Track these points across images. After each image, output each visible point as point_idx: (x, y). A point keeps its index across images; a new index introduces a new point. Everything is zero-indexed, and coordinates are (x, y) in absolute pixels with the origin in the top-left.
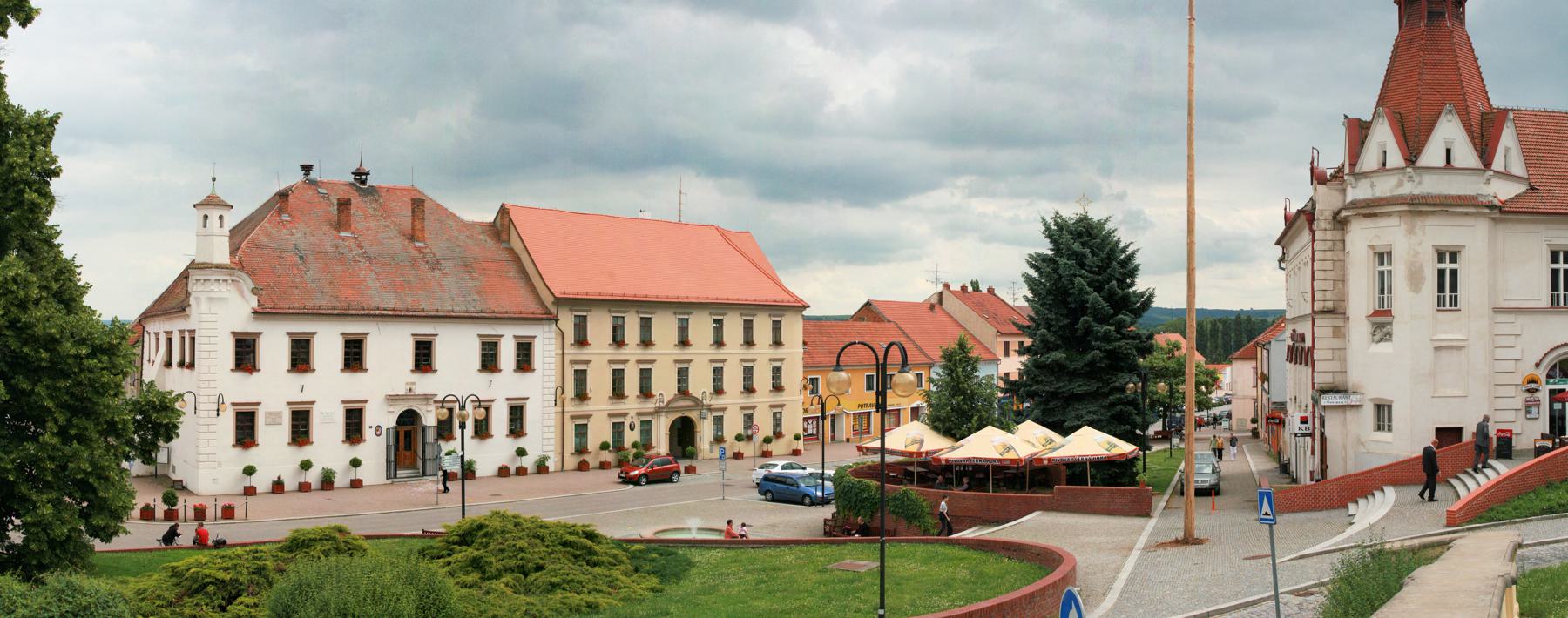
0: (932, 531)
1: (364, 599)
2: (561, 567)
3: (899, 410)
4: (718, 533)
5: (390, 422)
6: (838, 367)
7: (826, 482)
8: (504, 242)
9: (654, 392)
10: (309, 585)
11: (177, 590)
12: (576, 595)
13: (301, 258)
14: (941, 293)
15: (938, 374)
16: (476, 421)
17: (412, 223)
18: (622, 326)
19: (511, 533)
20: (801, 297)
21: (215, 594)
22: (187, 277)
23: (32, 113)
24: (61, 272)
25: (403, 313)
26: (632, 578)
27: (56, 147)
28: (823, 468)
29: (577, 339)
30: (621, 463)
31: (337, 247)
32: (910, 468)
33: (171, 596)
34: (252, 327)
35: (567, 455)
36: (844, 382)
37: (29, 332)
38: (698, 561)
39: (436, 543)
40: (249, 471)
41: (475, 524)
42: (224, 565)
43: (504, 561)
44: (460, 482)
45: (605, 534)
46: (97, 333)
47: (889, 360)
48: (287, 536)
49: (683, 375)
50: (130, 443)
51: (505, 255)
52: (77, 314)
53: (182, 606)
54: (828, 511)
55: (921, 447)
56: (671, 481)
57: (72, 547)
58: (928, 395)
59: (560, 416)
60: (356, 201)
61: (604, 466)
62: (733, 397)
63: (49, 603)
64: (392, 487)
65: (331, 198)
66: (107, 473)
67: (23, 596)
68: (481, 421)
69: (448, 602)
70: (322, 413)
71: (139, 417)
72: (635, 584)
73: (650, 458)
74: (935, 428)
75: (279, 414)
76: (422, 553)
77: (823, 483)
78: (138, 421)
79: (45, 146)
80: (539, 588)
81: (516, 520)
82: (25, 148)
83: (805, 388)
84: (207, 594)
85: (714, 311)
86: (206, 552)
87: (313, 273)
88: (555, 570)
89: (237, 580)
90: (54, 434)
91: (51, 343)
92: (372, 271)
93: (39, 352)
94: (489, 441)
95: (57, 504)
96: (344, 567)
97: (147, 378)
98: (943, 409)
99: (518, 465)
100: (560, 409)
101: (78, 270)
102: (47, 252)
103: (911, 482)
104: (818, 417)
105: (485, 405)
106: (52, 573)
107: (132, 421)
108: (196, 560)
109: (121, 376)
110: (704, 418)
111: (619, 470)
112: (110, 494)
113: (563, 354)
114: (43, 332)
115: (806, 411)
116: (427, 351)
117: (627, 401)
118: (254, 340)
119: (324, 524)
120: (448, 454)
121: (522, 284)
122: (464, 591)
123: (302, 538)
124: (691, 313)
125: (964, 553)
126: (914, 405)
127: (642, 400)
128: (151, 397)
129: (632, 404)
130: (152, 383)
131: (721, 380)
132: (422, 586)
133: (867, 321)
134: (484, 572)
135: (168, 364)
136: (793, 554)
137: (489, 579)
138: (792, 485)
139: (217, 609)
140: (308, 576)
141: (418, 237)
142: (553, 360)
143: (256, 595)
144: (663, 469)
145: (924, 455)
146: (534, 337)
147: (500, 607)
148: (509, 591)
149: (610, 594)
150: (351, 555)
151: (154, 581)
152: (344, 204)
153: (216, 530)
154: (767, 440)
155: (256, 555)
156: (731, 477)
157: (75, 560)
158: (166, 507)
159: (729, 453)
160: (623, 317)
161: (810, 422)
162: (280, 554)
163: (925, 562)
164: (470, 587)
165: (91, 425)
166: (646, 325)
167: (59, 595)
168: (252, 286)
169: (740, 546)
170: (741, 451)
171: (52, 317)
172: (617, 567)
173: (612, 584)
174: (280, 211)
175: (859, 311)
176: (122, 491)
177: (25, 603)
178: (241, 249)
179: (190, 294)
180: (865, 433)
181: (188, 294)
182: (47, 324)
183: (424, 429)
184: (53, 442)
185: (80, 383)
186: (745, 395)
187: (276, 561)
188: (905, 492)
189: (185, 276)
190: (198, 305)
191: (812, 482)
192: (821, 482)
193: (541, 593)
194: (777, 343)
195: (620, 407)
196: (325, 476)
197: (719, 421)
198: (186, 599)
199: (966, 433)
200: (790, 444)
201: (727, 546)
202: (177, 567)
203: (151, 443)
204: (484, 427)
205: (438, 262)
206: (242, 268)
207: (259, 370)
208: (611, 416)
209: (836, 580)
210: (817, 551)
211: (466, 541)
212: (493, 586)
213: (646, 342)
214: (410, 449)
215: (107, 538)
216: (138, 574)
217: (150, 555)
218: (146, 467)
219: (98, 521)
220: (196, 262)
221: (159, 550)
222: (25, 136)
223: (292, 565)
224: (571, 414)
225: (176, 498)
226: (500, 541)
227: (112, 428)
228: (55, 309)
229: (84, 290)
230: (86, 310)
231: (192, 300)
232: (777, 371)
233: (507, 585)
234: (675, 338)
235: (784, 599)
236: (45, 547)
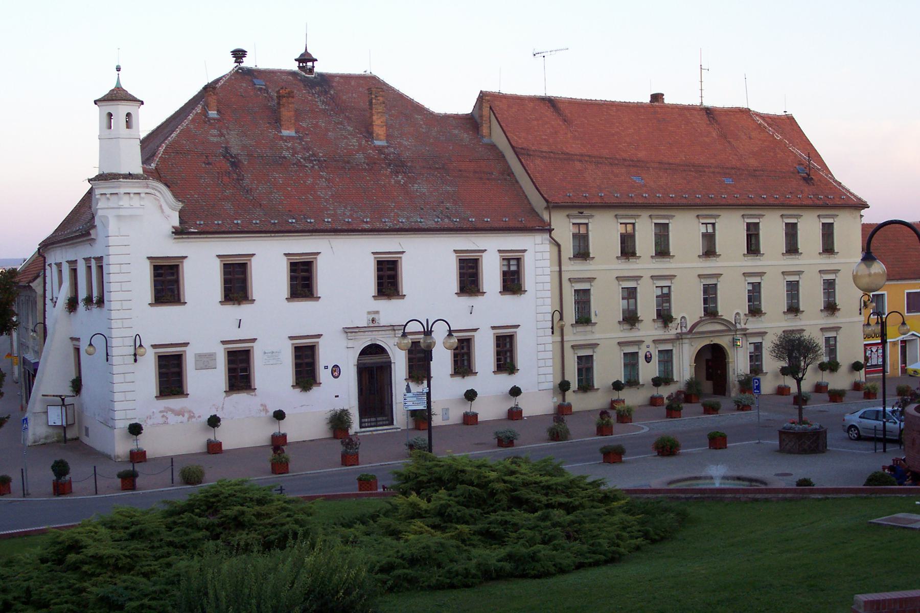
9: (674, 315)
34: (171, 249)
49: (710, 293)
100: (559, 339)
113: (560, 271)
142: (548, 279)
160: (587, 224)
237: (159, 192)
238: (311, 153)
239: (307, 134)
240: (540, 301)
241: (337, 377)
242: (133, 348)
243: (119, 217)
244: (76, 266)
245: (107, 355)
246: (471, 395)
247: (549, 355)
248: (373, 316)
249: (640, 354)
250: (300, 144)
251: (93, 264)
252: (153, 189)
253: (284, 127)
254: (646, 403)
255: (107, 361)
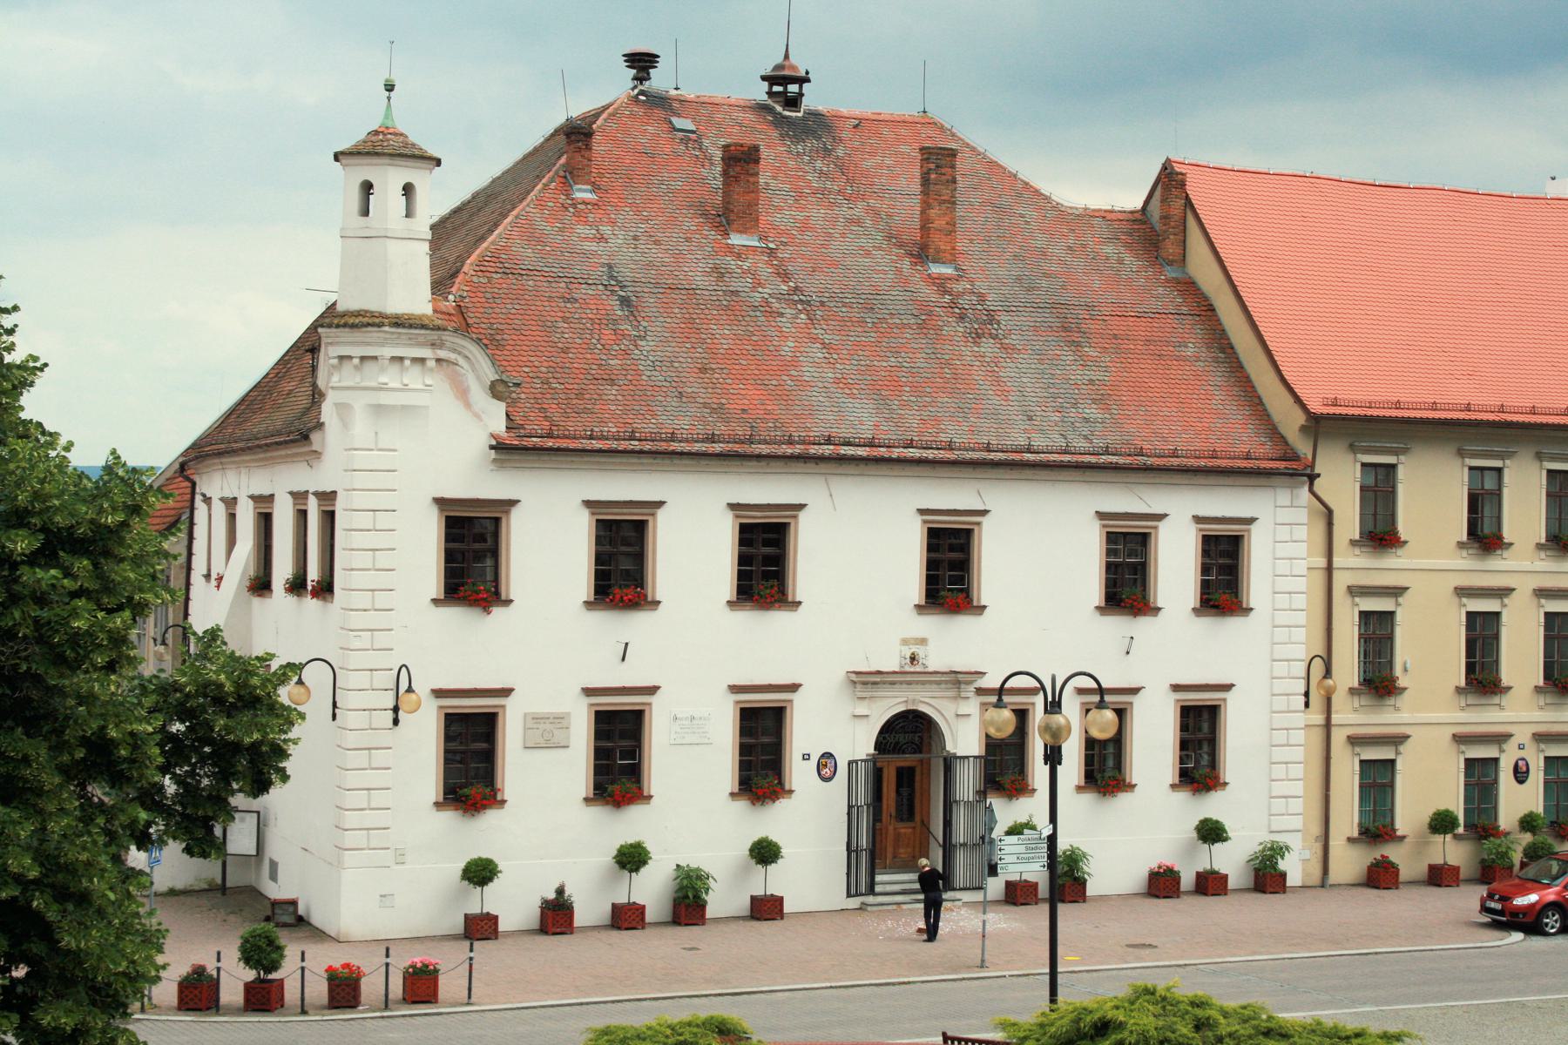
34: (487, 485)
70: (676, 718)
113: (1329, 569)
142: (1301, 584)
160: (1499, 470)
237: (466, 357)
238: (791, 284)
240: (1281, 634)
241: (829, 779)
242: (392, 694)
243: (379, 410)
244: (272, 508)
245: (335, 705)
247: (1298, 754)
248: (914, 649)
249: (1502, 763)
251: (313, 509)
252: (454, 351)
254: (1422, 879)
255: (334, 717)
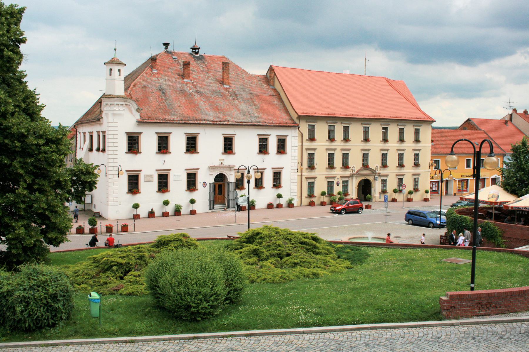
0: (502, 246)
1: (196, 270)
2: (300, 255)
3: (484, 179)
4: (382, 240)
5: (211, 180)
6: (452, 153)
7: (442, 216)
8: (271, 85)
9: (350, 166)
10: (167, 264)
11: (97, 269)
12: (307, 269)
13: (163, 93)
14: (511, 115)
15: (509, 159)
16: (256, 179)
17: (223, 75)
18: (334, 131)
19: (274, 237)
20: (431, 116)
21: (117, 271)
22: (101, 103)
23: (8, 6)
24: (27, 97)
25: (218, 123)
26: (337, 261)
27: (23, 25)
28: (441, 208)
29: (310, 137)
30: (332, 203)
31: (183, 88)
32: (490, 211)
33: (93, 273)
35: (303, 198)
36: (455, 161)
37: (8, 131)
38: (372, 254)
39: (234, 242)
40: (136, 206)
41: (255, 232)
42: (122, 255)
43: (270, 251)
44: (247, 211)
45: (323, 239)
46: (49, 132)
47: (482, 152)
48: (156, 240)
49: (365, 157)
50: (69, 192)
51: (271, 92)
52: (37, 121)
53: (99, 278)
54: (443, 232)
55: (497, 200)
56: (358, 213)
57: (37, 250)
58: (502, 171)
59: (300, 177)
60: (193, 63)
61: (323, 204)
62: (392, 169)
63: (22, 282)
64: (211, 214)
65: (179, 61)
66: (56, 209)
67: (7, 279)
68: (259, 179)
69: (240, 272)
70: (174, 175)
71: (74, 178)
72: (338, 264)
73: (347, 200)
74: (506, 190)
75: (151, 176)
76: (227, 247)
77: (440, 217)
78: (73, 180)
79: (17, 25)
80: (288, 265)
81: (276, 230)
82: (4, 25)
83: (432, 165)
84: (113, 271)
85: (383, 123)
86: (112, 249)
87: (169, 102)
88: (296, 256)
89: (129, 263)
90: (24, 189)
91: (22, 137)
92: (201, 100)
93: (15, 143)
94: (262, 190)
95: (27, 227)
96: (186, 254)
97: (78, 158)
98: (511, 179)
99: (278, 203)
100: (300, 174)
101: (37, 97)
102: (18, 86)
103: (491, 218)
104: (439, 181)
105: (261, 171)
106: (25, 264)
107: (70, 180)
108: (107, 253)
109: (63, 156)
110: (377, 180)
111: (331, 206)
112: (58, 220)
113: (302, 145)
114: (17, 131)
115: (432, 178)
116: (230, 143)
117: (335, 170)
118: (138, 137)
119: (175, 233)
120: (241, 196)
121: (281, 108)
122: (249, 267)
123: (164, 240)
124: (370, 124)
125: (521, 259)
126: (493, 177)
127: (343, 170)
128: (81, 167)
129: (338, 172)
130: (81, 160)
131: (386, 160)
132: (227, 263)
133: (468, 130)
134: (259, 257)
135: (91, 150)
136: (423, 252)
137: (262, 260)
138: (423, 217)
139: (119, 279)
140: (167, 259)
141: (226, 83)
142: (297, 148)
143: (140, 270)
144: (354, 206)
145: (498, 204)
146: (287, 136)
147: (268, 274)
148: (272, 266)
149: (325, 269)
150: (190, 248)
151: (83, 266)
152: (186, 65)
153: (119, 238)
154: (410, 193)
155: (139, 250)
156: (390, 211)
157: (38, 257)
158: (91, 227)
159: (389, 199)
160: (334, 126)
161: (434, 184)
162: (152, 249)
163: (498, 261)
164: (252, 264)
165: (46, 183)
166: (346, 130)
167: (29, 276)
168: (137, 108)
169: (395, 247)
170: (396, 198)
171: (22, 123)
172: (329, 255)
173: (326, 264)
174: (152, 68)
175: (463, 124)
176: (65, 218)
177: (8, 282)
178: (130, 88)
179: (102, 112)
180: (464, 191)
181: (101, 112)
182: (19, 127)
183: (229, 184)
184: (24, 193)
185: (39, 160)
186: (399, 168)
187: (149, 252)
188: (487, 223)
189: (99, 102)
190: (107, 118)
191: (434, 215)
192: (439, 216)
193: (289, 267)
194: (417, 141)
195: (332, 173)
196: (176, 209)
197: (384, 182)
198: (101, 274)
199: (524, 193)
200: (422, 195)
201: (387, 247)
202: (97, 258)
203: (81, 192)
204: (260, 183)
205: (236, 96)
206: (131, 98)
207: (141, 153)
208: (327, 178)
209: (447, 268)
210: (436, 251)
211: (250, 241)
212: (264, 264)
213: (346, 139)
214: (221, 194)
215: (57, 244)
216: (75, 263)
217: (82, 252)
218: (78, 205)
219: (52, 235)
220: (106, 94)
221: (86, 249)
222: (4, 19)
223: (159, 255)
224: (306, 176)
225: (96, 222)
226: (268, 241)
227: (59, 184)
228: (24, 118)
229: (41, 108)
230: (42, 119)
231: (104, 115)
232: (417, 156)
233: (271, 263)
234: (361, 137)
235: (418, 275)
236: (21, 252)
239: (195, 81)
246: (279, 196)
249: (334, 182)
250: (192, 85)
252: (129, 103)
253: (185, 77)
